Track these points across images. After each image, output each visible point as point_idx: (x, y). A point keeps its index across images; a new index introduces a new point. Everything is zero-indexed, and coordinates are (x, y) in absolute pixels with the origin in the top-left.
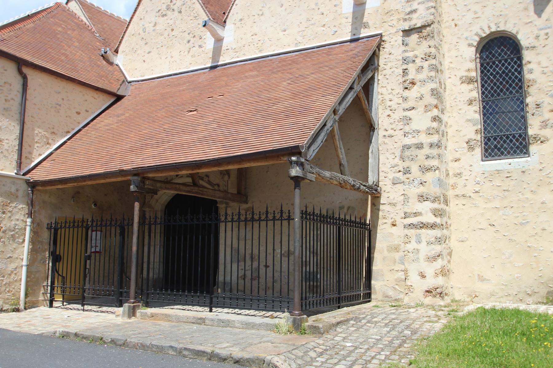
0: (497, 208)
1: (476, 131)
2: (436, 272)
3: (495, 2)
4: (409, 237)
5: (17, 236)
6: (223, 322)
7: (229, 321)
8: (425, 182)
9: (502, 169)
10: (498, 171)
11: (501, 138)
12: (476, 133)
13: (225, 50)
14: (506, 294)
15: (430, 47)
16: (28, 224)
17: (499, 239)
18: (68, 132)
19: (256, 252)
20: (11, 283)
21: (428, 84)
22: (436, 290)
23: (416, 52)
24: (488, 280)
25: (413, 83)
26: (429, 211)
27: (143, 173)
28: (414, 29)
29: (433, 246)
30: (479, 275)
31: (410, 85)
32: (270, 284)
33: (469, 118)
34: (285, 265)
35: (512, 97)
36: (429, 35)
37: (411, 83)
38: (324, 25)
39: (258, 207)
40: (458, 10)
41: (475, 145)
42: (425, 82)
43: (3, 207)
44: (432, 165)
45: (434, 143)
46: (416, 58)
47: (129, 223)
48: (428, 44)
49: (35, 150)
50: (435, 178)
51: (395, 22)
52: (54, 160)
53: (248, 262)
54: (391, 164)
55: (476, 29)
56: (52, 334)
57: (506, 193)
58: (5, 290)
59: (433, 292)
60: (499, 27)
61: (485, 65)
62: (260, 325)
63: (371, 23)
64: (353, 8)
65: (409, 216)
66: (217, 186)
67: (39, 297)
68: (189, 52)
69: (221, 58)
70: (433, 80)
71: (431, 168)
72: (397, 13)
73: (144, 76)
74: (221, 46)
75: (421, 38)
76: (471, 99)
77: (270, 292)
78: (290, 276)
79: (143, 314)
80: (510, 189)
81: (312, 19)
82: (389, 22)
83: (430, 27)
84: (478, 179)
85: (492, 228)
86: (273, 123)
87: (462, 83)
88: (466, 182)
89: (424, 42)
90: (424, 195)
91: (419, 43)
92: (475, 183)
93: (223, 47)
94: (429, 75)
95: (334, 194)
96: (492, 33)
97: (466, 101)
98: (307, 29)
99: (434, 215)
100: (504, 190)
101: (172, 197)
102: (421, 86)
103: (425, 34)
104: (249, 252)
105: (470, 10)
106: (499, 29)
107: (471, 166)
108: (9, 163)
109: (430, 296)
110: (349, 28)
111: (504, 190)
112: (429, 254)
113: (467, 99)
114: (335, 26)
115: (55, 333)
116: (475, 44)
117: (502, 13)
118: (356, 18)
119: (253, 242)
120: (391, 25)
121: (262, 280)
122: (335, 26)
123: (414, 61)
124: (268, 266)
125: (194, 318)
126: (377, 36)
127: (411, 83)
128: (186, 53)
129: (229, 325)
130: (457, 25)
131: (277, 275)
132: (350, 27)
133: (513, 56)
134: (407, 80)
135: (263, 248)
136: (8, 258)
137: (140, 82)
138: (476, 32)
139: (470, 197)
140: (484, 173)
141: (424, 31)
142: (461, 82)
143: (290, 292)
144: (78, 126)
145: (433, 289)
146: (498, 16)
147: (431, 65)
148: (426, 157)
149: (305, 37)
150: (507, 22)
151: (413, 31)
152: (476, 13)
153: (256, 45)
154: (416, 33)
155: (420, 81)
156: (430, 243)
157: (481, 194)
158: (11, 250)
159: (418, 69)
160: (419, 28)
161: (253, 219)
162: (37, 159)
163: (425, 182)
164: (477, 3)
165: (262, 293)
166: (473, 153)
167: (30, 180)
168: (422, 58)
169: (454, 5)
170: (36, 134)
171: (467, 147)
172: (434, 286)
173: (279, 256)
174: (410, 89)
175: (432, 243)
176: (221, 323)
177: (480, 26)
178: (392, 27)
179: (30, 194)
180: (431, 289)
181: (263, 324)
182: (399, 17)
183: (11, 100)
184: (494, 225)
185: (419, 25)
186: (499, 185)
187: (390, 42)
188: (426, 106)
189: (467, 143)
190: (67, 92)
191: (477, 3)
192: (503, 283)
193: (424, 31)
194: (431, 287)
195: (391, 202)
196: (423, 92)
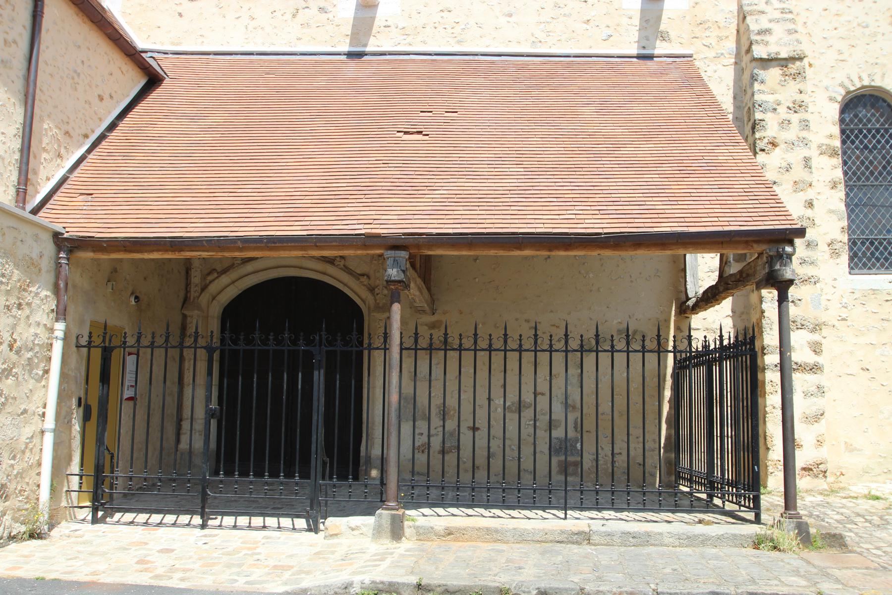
0: (872, 344)
1: (843, 228)
2: (819, 439)
3: (868, 43)
4: (775, 384)
5: (36, 361)
6: (633, 537)
7: (648, 534)
8: (800, 300)
9: (879, 288)
10: (874, 290)
11: (872, 243)
12: (842, 232)
13: (382, 28)
14: (886, 471)
15: (801, 93)
16: (60, 334)
17: (876, 389)
18: (86, 136)
19: (452, 402)
20: (25, 471)
21: (798, 148)
22: (818, 468)
23: (777, 97)
24: (859, 450)
25: (774, 144)
26: (806, 344)
27: (418, 246)
28: (776, 59)
29: (813, 399)
30: (846, 443)
31: (770, 146)
32: (481, 460)
33: (833, 208)
34: (512, 428)
35: (886, 186)
36: (800, 74)
37: (770, 143)
38: (588, 21)
39: (456, 322)
40: (813, 43)
41: (841, 250)
42: (793, 144)
43: (19, 292)
44: (810, 275)
45: (812, 242)
46: (778, 105)
47: (154, 342)
48: (798, 86)
49: (42, 167)
50: (816, 294)
51: (713, 41)
52: (91, 194)
53: (436, 422)
54: (709, 267)
55: (841, 77)
56: (337, 590)
57: (885, 324)
58: (16, 489)
59: (814, 469)
60: (873, 80)
61: (848, 132)
62: (719, 538)
63: (672, 34)
64: (642, 3)
65: (773, 350)
66: (365, 277)
67: (60, 502)
68: (294, 16)
69: (372, 40)
70: (807, 145)
71: (809, 278)
72: (717, 28)
73: (179, 44)
74: (373, 19)
75: (786, 75)
76: (834, 180)
77: (481, 475)
78: (521, 446)
79: (421, 531)
80: (890, 318)
81: (563, 6)
82: (703, 39)
83: (801, 62)
84: (845, 300)
85: (866, 373)
86: (99, 161)
87: (822, 154)
88: (827, 303)
89: (792, 83)
90: (799, 320)
91: (783, 83)
92: (841, 306)
93: (377, 20)
94: (800, 136)
95: (608, 307)
96: (863, 87)
97: (827, 181)
98: (555, 21)
99: (815, 351)
100: (883, 320)
101: (240, 292)
102: (787, 151)
103: (793, 71)
104: (437, 401)
105: (831, 46)
106: (873, 84)
107: (835, 279)
108: (4, 189)
109: (808, 477)
110: (634, 35)
111: (883, 320)
112: (808, 412)
113: (830, 179)
114: (608, 27)
115: (346, 588)
116: (839, 99)
117: (878, 61)
118: (647, 21)
119: (447, 384)
120: (706, 44)
121: (466, 453)
122: (608, 27)
123: (775, 109)
124: (478, 429)
125: (563, 532)
126: (684, 57)
127: (770, 143)
128: (288, 16)
129: (648, 541)
130: (813, 66)
131: (496, 445)
132: (637, 34)
133: (889, 125)
134: (764, 138)
135: (467, 396)
136: (22, 413)
137: (170, 56)
138: (840, 82)
139: (834, 326)
140: (853, 293)
141: (790, 65)
142: (819, 152)
143: (522, 473)
144: (99, 126)
145: (814, 465)
146: (872, 64)
147: (804, 121)
148: (800, 261)
149: (551, 34)
150: (886, 76)
151: (773, 63)
152: (840, 52)
153: (450, 30)
154: (778, 66)
155: (786, 143)
156: (809, 394)
157: (849, 323)
158: (26, 394)
159: (782, 122)
160: (785, 59)
161: (446, 347)
162: (43, 187)
163: (800, 300)
164: (842, 38)
165: (466, 477)
166: (838, 261)
167: (63, 234)
168: (789, 108)
169: (808, 35)
170: (46, 130)
171: (828, 251)
172: (815, 460)
173: (500, 410)
174: (769, 152)
175: (812, 395)
176: (631, 539)
177: (847, 74)
178: (709, 47)
179: (63, 265)
180: (811, 465)
181: (726, 536)
182: (720, 35)
183: (12, 44)
184: (868, 370)
185: (784, 55)
186: (875, 311)
187: (706, 71)
188: (795, 182)
189: (829, 246)
190: (89, 49)
191: (842, 38)
192: (879, 454)
193: (790, 65)
194: (811, 462)
195: (709, 327)
196: (791, 160)
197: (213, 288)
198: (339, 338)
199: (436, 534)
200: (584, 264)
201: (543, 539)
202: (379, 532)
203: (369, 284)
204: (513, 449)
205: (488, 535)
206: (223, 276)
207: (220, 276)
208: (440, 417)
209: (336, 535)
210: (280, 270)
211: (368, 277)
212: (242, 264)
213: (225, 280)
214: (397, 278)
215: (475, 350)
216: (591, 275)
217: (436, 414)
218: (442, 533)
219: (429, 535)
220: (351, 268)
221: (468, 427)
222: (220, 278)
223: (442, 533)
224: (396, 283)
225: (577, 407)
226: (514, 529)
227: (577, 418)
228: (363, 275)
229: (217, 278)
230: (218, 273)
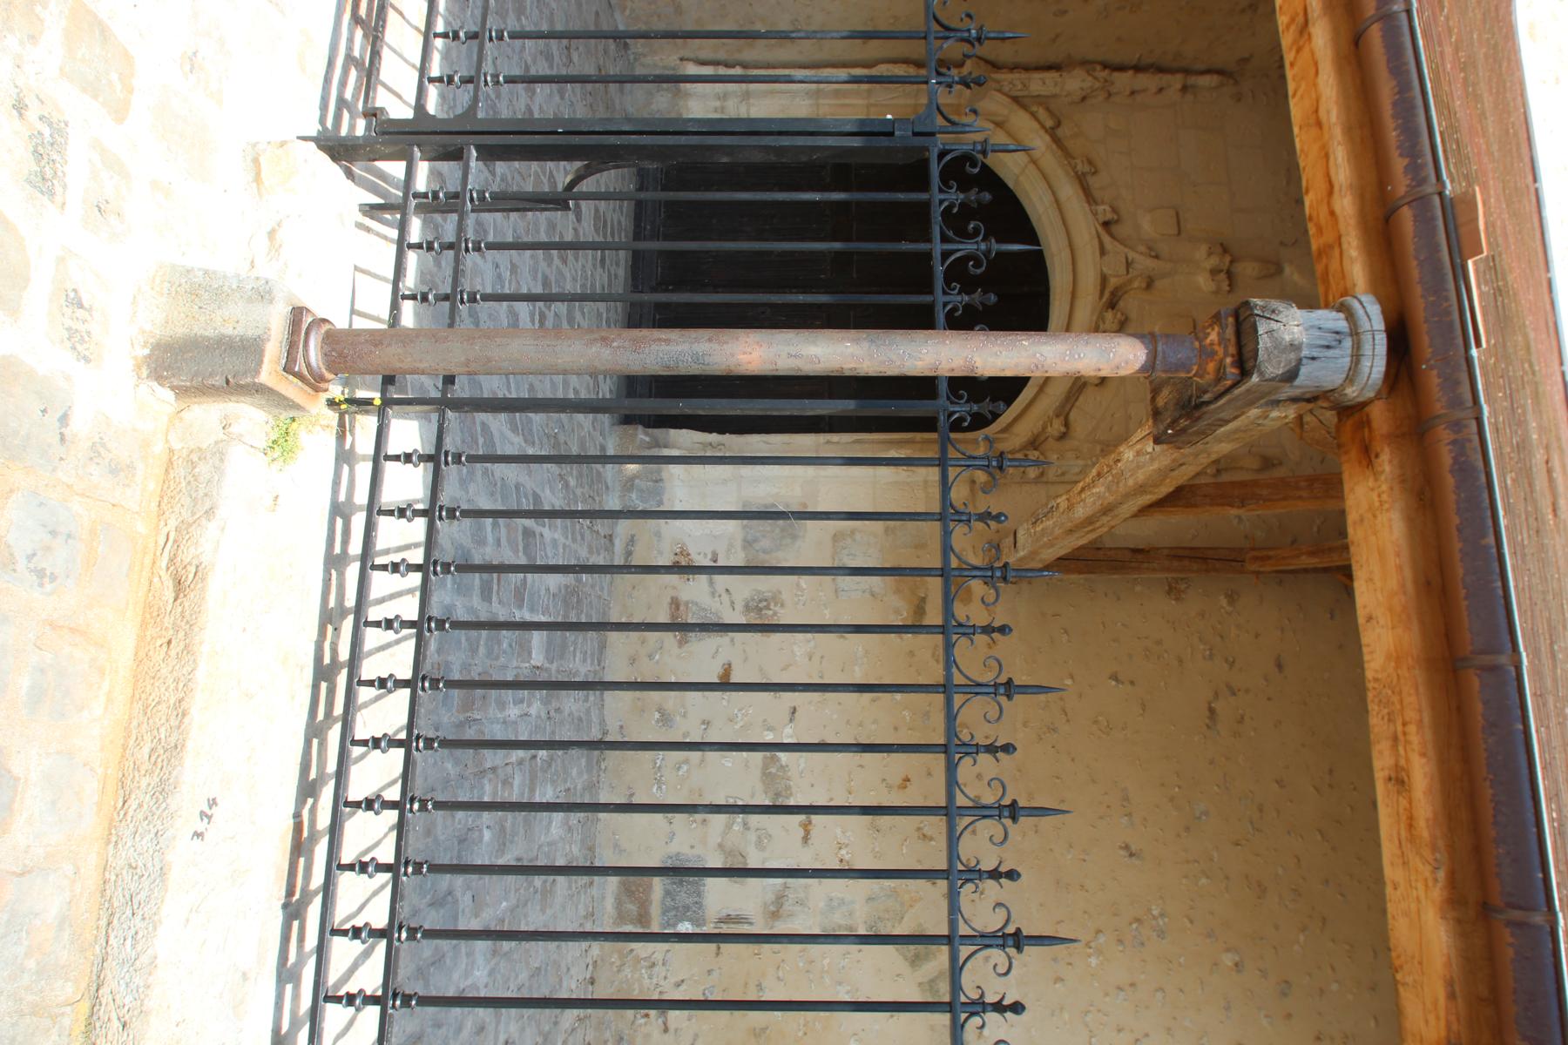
66: (1063, 429)
101: (1011, 185)
197: (1022, 122)
198: (973, 195)
199: (184, 528)
200: (1120, 941)
201: (107, 1010)
202: (194, 292)
203: (1047, 438)
204: (679, 769)
205: (153, 750)
206: (1047, 138)
207: (1046, 131)
208: (753, 600)
209: (258, 178)
210: (1066, 254)
211: (1063, 437)
212: (1076, 173)
213: (1039, 142)
214: (1264, 342)
215: (946, 688)
216: (1093, 961)
217: (759, 592)
218: (187, 555)
219: (187, 501)
220: (1081, 399)
221: (730, 665)
222: (1042, 132)
223: (187, 555)
224: (1232, 350)
225: (777, 923)
226: (163, 872)
227: (751, 924)
228: (1067, 424)
229: (1043, 127)
230: (1052, 128)
